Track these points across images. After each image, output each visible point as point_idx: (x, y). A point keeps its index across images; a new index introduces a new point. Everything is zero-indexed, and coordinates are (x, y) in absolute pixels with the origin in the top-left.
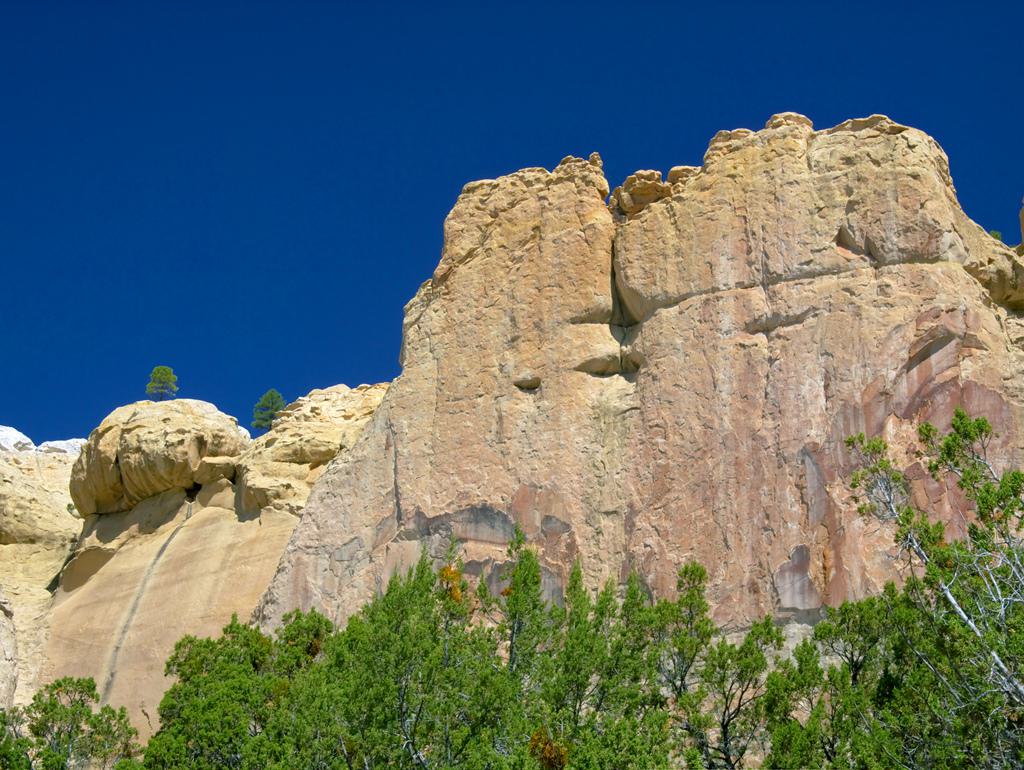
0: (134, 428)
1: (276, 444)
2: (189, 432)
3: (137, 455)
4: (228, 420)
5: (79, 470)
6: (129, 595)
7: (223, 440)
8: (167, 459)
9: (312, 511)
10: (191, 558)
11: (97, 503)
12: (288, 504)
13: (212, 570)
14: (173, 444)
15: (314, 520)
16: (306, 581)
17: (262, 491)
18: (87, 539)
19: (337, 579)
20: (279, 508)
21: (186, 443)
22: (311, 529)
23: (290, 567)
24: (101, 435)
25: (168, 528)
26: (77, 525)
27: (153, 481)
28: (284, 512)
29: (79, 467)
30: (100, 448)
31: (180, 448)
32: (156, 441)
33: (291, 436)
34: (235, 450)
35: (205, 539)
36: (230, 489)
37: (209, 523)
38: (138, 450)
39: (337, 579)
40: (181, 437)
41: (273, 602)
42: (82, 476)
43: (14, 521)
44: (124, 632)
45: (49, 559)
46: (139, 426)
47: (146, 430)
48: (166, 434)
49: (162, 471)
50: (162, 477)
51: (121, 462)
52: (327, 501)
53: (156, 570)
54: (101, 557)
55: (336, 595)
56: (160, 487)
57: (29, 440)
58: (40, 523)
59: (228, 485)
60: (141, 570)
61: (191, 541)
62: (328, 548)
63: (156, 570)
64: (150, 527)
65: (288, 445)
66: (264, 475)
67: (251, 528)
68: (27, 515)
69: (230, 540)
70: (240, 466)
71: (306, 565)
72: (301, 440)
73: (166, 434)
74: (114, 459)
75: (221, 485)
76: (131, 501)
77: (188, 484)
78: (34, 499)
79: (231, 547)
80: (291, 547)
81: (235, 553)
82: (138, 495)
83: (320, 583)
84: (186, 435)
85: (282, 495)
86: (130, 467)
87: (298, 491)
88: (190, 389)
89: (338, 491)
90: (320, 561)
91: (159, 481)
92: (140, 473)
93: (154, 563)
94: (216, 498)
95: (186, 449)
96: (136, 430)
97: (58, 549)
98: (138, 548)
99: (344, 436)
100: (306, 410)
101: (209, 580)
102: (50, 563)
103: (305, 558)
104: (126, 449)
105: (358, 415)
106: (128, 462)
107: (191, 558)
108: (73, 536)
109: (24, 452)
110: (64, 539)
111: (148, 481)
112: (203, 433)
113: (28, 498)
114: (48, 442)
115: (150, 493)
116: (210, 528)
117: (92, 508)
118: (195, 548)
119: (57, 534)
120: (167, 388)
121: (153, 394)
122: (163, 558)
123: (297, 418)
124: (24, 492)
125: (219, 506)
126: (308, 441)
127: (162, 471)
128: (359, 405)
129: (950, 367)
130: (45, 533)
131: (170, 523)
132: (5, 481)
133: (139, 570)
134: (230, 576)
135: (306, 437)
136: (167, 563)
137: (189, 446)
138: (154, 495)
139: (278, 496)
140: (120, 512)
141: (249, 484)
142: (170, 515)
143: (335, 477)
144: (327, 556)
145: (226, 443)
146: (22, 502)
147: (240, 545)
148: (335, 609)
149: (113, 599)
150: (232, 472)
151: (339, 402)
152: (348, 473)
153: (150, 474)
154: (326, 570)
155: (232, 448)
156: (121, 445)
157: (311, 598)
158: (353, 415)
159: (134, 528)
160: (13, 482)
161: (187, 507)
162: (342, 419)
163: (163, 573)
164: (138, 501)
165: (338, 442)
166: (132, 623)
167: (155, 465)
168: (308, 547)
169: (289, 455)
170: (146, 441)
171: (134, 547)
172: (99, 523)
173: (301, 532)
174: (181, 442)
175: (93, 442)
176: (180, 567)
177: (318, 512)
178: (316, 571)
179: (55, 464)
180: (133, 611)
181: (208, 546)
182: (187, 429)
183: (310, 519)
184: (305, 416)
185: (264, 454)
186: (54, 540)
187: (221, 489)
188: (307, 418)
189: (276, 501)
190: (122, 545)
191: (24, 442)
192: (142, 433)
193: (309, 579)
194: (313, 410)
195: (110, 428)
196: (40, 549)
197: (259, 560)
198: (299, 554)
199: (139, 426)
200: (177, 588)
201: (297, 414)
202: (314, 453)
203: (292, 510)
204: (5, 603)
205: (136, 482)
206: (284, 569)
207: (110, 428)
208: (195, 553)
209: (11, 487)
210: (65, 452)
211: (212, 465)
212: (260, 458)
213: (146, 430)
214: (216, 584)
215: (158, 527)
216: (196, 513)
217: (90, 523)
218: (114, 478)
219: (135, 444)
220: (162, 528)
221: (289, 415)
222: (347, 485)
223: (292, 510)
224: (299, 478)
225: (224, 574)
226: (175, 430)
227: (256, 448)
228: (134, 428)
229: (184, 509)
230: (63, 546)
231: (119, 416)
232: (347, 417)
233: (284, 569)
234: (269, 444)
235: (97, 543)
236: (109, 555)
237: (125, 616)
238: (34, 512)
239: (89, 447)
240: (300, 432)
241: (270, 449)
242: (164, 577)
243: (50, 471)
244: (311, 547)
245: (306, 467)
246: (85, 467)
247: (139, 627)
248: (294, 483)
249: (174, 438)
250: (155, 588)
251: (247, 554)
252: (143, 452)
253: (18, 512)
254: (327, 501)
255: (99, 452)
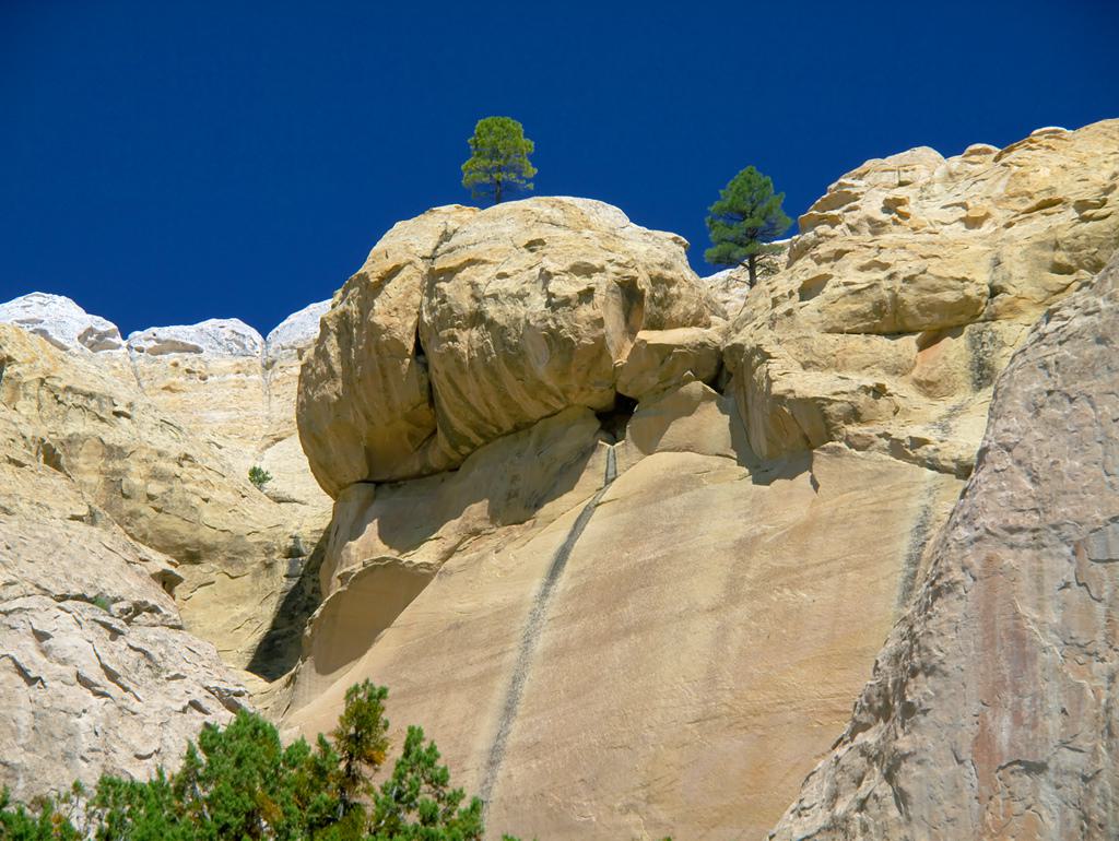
0: (461, 268)
1: (828, 289)
2: (602, 270)
3: (475, 334)
4: (669, 243)
5: (323, 378)
6: (492, 674)
7: (674, 290)
8: (553, 338)
9: (1012, 438)
10: (642, 577)
11: (370, 455)
12: (886, 436)
13: (705, 602)
14: (566, 302)
15: (1019, 463)
16: (1017, 616)
17: (814, 407)
18: (354, 544)
19: (1100, 608)
20: (864, 445)
21: (598, 298)
22: (1014, 484)
23: (970, 582)
24: (375, 289)
25: (564, 508)
26: (313, 511)
27: (518, 394)
28: (878, 455)
29: (322, 368)
30: (378, 319)
31: (585, 311)
32: (521, 296)
33: (863, 269)
34: (700, 314)
35: (673, 528)
36: (713, 405)
37: (670, 492)
38: (477, 319)
39: (1100, 608)
40: (583, 283)
41: (930, 671)
42: (332, 390)
43: (147, 509)
44: (492, 763)
45: (240, 599)
46: (471, 262)
47: (491, 271)
48: (546, 276)
49: (542, 367)
50: (541, 385)
51: (434, 351)
52: (1050, 412)
53: (552, 609)
54: (395, 587)
55: (1102, 648)
56: (533, 409)
57: (112, 326)
58: (207, 514)
59: (707, 397)
60: (511, 611)
61: (633, 535)
62: (1067, 531)
63: (552, 609)
64: (518, 507)
65: (858, 292)
66: (805, 366)
67: (791, 499)
68: (177, 495)
69: (741, 529)
70: (738, 348)
71: (1012, 575)
72: (891, 277)
73: (546, 276)
74: (410, 345)
75: (689, 397)
76: (455, 447)
77: (601, 398)
78: (186, 457)
79: (745, 546)
80: (963, 533)
81: (760, 561)
82: (476, 429)
83: (1055, 618)
84: (597, 277)
85: (867, 413)
86: (459, 361)
87: (901, 403)
88: (560, 175)
89: (1081, 385)
90: (1047, 563)
91: (533, 395)
92: (483, 377)
93: (545, 594)
94: (678, 429)
95: (599, 313)
96: (467, 272)
97: (256, 574)
98: (494, 559)
99: (997, 263)
100: (872, 206)
101: (701, 631)
102: (243, 609)
103: (1007, 557)
104: (447, 318)
105: (1000, 215)
106: (452, 351)
107: (642, 577)
108: (290, 543)
109: (102, 354)
110: (269, 551)
111: (505, 397)
112: (632, 272)
113: (175, 454)
114: (154, 329)
115: (508, 425)
116: (677, 502)
117: (357, 468)
118: (648, 552)
119: (251, 539)
120: (512, 169)
121: (481, 186)
122: (564, 582)
123: (852, 229)
124: (162, 441)
125: (687, 449)
126: (910, 279)
127: (542, 367)
128: (999, 190)
129: (386, 390)
130: (222, 538)
131: (567, 497)
132: (118, 414)
133: (506, 613)
134: (756, 615)
135: (904, 269)
136: (581, 592)
137: (605, 304)
138: (517, 429)
139: (854, 415)
140: (425, 475)
141: (777, 388)
142: (564, 477)
143: (1066, 351)
144: (1067, 550)
145: (679, 297)
146: (162, 464)
147: (769, 539)
148: (1103, 683)
149: (447, 686)
150: (715, 363)
151: (937, 188)
152: (1101, 340)
153: (508, 376)
154: (1067, 585)
155: (693, 308)
156: (432, 309)
157: (1034, 658)
158: (988, 216)
159: (477, 511)
160: (136, 415)
161: (604, 453)
162: (961, 226)
163: (575, 617)
164: (474, 447)
165: (983, 277)
166: (512, 740)
167: (522, 354)
168: (1012, 530)
169: (865, 315)
170: (495, 296)
171: (481, 558)
172: (375, 507)
173: (989, 493)
174: (587, 295)
175: (354, 307)
176: (617, 600)
177: (1028, 441)
178: (1040, 589)
179: (179, 380)
180: (509, 710)
181: (681, 547)
182: (596, 263)
183: (1007, 461)
184: (871, 221)
185: (801, 315)
186: (244, 553)
187: (689, 407)
188: (877, 227)
189: (853, 429)
190: (450, 553)
191: (101, 329)
192: (483, 276)
193: (1026, 610)
194: (891, 206)
195: (397, 270)
196: (214, 577)
197: (828, 575)
198: (989, 548)
199: (471, 262)
200: (618, 651)
201: (851, 218)
202: (928, 308)
203: (897, 448)
204: (239, 694)
205: (473, 401)
206: (951, 588)
207: (397, 270)
208: (652, 564)
209: (133, 429)
210: (197, 350)
211: (664, 350)
212: (792, 326)
213: (491, 271)
214: (723, 633)
215: (538, 506)
216: (629, 472)
217: (353, 507)
218: (416, 394)
219: (467, 305)
220: (547, 509)
221: (834, 222)
222: (1102, 370)
223: (897, 448)
224: (897, 370)
225: (740, 612)
226: (566, 267)
227: (775, 302)
228: (461, 268)
229: (599, 461)
230: (269, 566)
231: (407, 242)
232: (972, 223)
233: (951, 588)
234: (809, 290)
235: (383, 551)
236: (418, 579)
237: (487, 727)
238: (188, 486)
239: (343, 319)
240: (883, 258)
241: (813, 303)
242: (577, 627)
243: (167, 397)
244: (1020, 530)
245: (909, 343)
246: (338, 368)
247: (532, 749)
248: (890, 384)
249: (566, 287)
250: (558, 653)
251: (793, 561)
252: (491, 324)
253: (155, 488)
254: (1050, 412)
255: (375, 329)
